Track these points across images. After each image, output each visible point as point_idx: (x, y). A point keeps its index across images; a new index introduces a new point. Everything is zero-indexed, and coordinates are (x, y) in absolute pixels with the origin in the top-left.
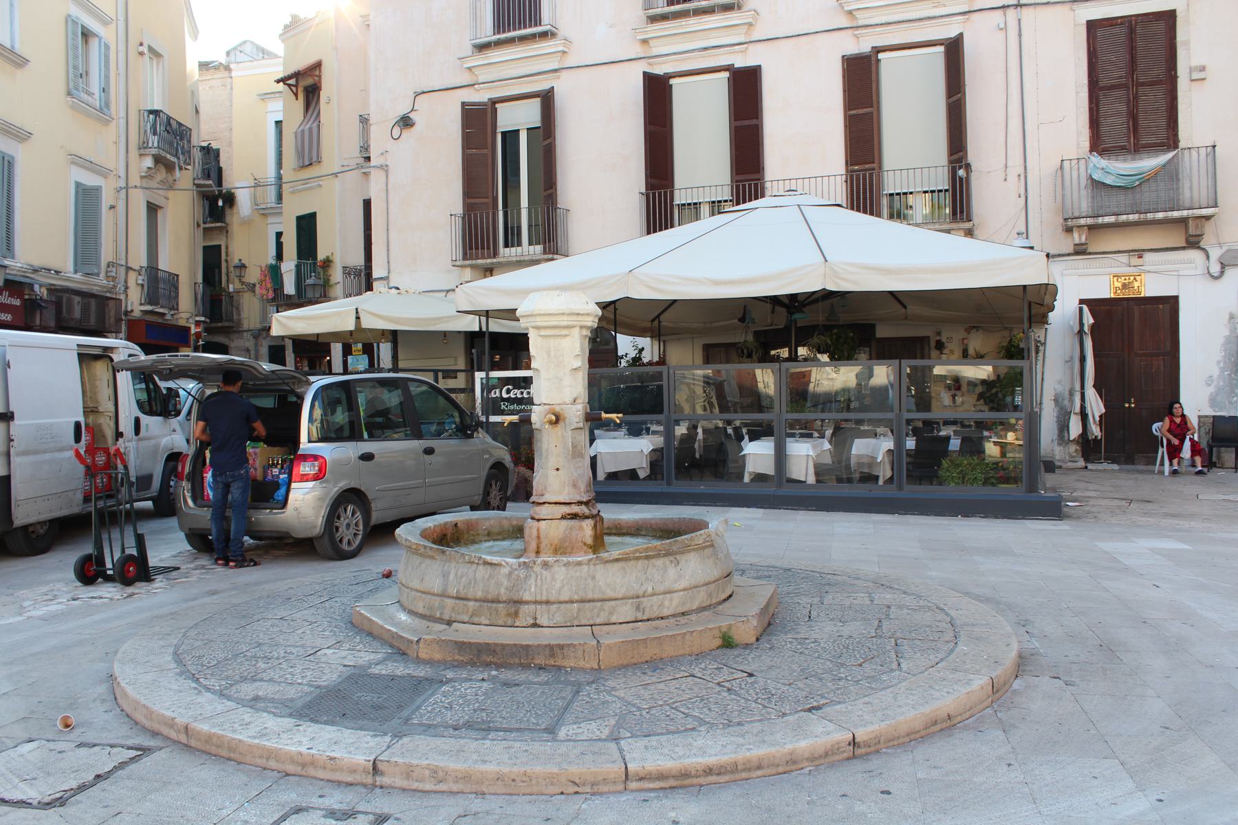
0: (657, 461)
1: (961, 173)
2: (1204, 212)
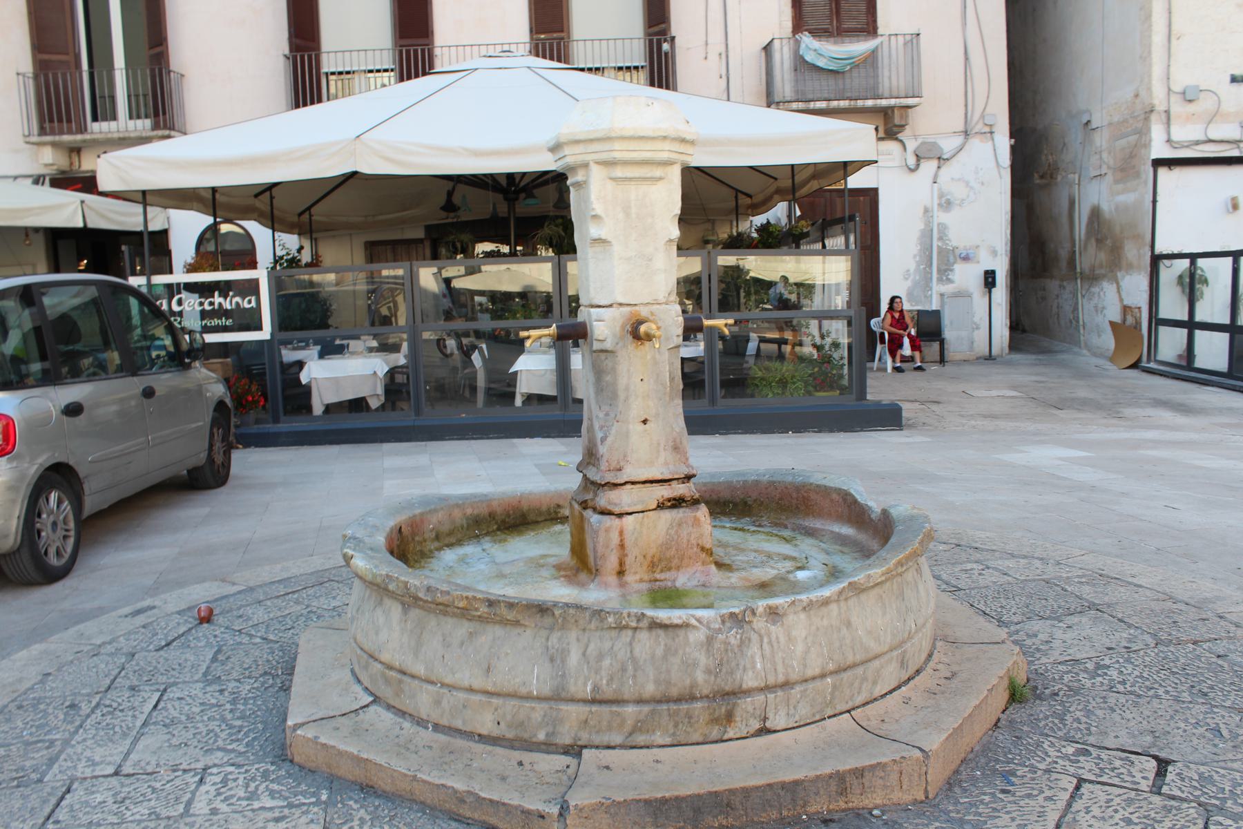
0: (395, 388)
1: (666, 46)
2: (910, 101)
